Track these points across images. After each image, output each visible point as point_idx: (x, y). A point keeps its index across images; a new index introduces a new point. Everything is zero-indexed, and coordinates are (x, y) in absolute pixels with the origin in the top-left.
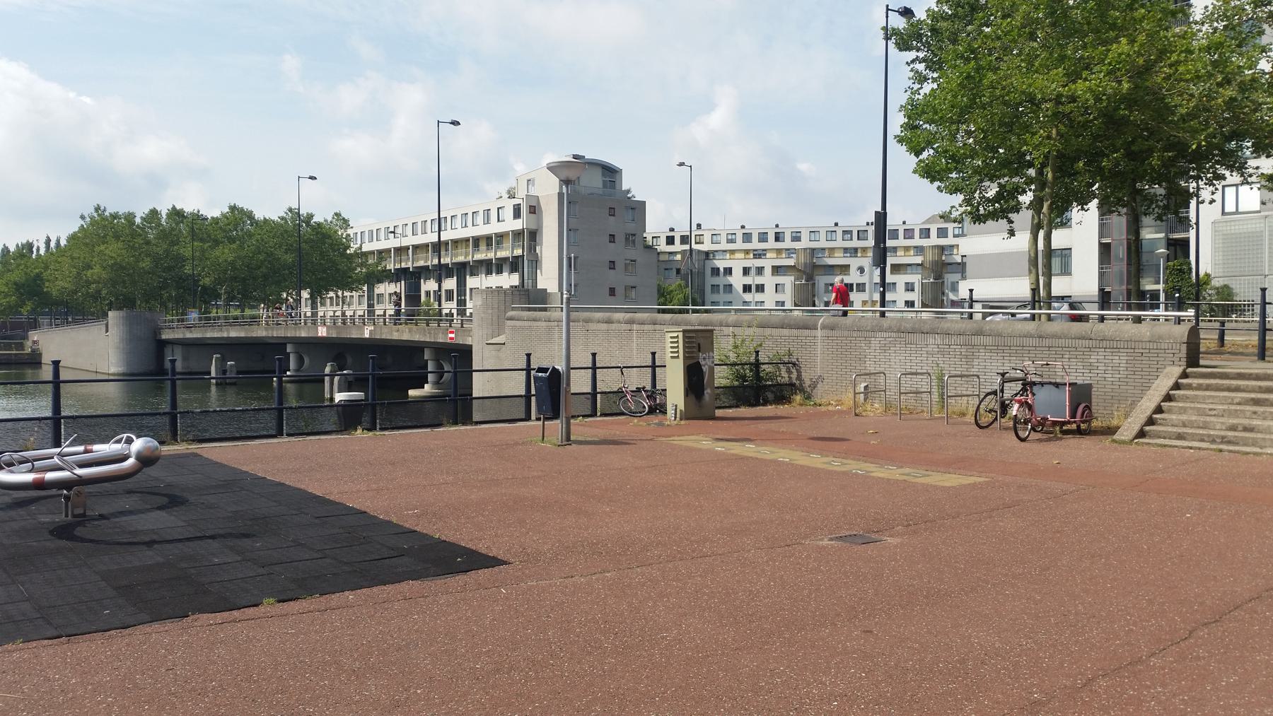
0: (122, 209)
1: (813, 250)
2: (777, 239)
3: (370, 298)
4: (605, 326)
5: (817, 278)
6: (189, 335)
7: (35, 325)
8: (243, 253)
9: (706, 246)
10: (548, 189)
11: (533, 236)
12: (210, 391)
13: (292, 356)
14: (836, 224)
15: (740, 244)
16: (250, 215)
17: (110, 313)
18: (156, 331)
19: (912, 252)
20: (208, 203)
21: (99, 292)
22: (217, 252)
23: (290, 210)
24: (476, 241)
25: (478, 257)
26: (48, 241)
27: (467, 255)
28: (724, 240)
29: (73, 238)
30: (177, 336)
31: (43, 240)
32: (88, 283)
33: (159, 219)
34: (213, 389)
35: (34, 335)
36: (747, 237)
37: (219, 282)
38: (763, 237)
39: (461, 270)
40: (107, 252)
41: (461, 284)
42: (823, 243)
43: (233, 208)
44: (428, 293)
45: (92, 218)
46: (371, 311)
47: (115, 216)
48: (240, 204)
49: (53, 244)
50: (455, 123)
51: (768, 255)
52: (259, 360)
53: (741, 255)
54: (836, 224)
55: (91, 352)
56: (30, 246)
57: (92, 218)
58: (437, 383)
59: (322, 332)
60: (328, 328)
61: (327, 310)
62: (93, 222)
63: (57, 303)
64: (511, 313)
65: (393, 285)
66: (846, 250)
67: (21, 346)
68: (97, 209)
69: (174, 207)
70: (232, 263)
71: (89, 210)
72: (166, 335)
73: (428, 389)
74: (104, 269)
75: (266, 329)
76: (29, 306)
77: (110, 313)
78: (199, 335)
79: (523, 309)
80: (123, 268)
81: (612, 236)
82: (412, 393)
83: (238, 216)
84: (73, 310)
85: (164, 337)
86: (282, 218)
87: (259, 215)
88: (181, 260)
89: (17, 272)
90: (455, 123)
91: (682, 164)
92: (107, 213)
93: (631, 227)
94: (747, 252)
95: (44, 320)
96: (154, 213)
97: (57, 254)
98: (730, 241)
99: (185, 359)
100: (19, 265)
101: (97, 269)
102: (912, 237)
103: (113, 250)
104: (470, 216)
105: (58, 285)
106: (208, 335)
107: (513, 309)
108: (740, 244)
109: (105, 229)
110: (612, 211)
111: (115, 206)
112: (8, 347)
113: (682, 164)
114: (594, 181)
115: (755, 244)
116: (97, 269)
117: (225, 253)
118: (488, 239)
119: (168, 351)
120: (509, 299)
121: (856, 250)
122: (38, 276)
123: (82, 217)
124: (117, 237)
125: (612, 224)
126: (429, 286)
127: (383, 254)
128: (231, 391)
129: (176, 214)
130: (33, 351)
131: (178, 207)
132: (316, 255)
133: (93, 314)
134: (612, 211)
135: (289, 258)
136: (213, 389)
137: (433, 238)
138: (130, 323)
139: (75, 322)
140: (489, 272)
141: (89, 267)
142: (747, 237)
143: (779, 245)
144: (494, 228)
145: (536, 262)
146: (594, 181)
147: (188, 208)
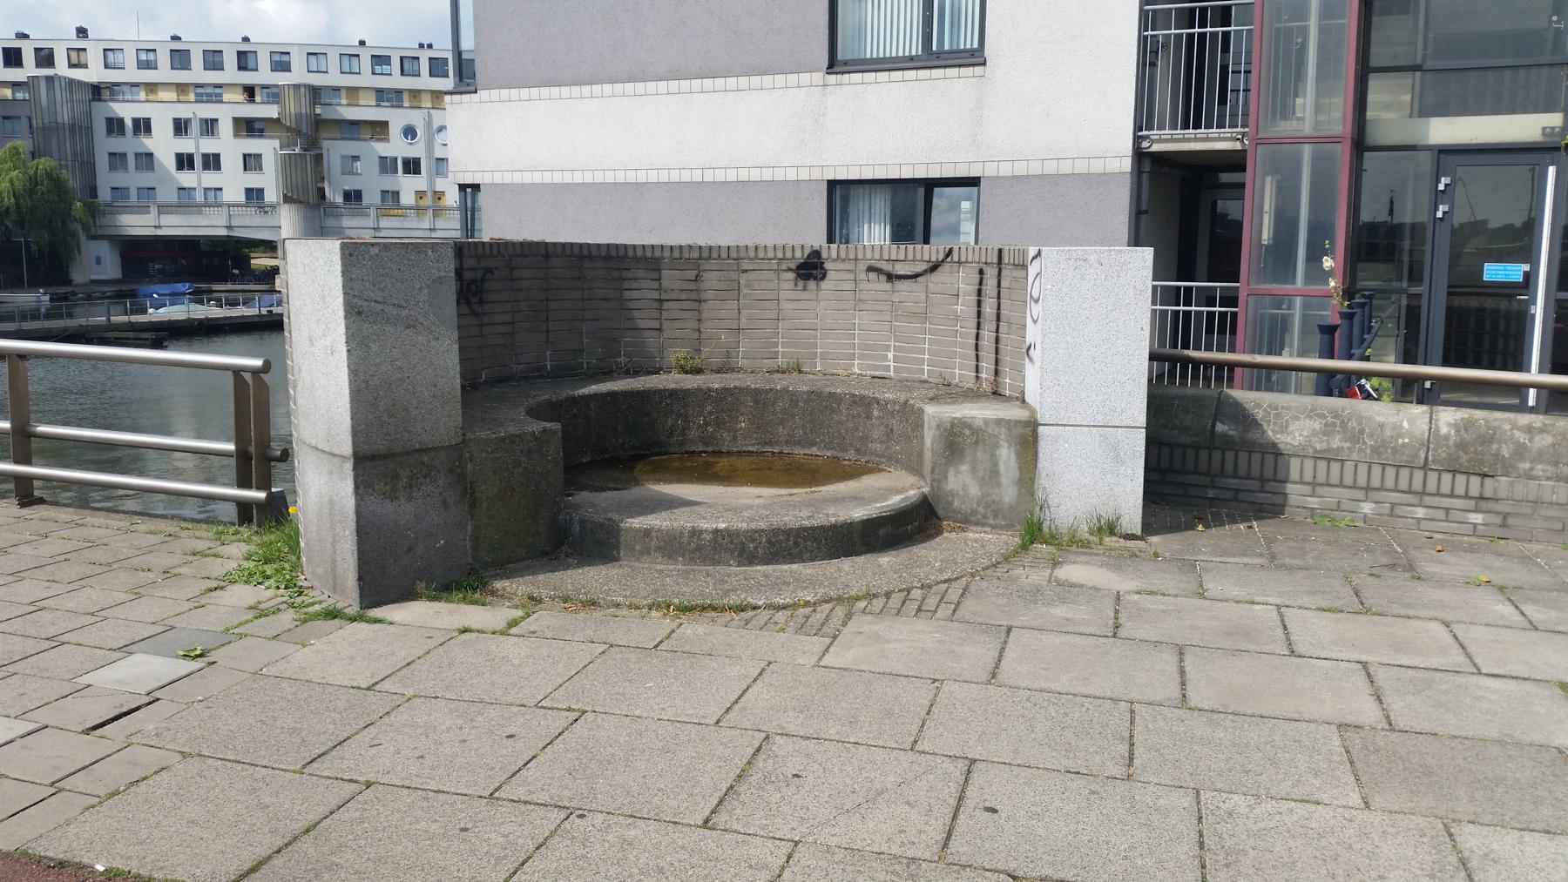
9: (94, 73)
42: (333, 78)
53: (172, 96)
54: (362, 43)
94: (182, 88)
108: (164, 73)
142: (180, 59)
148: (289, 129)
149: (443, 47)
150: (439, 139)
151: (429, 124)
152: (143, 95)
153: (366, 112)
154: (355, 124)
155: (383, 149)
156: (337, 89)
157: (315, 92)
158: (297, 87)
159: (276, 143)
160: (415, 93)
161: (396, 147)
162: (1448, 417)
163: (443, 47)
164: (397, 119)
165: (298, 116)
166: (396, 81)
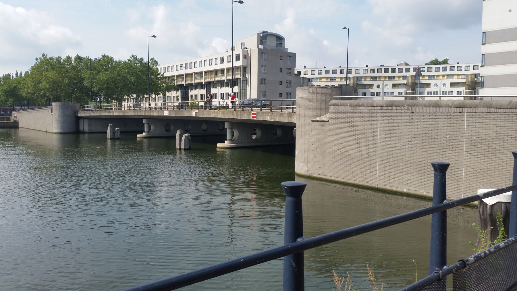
0: (55, 56)
1: (357, 77)
2: (385, 72)
3: (164, 98)
4: (432, 109)
5: (359, 90)
6: (92, 114)
7: (13, 110)
8: (112, 76)
9: (309, 76)
10: (253, 45)
11: (245, 69)
12: (105, 144)
13: (145, 125)
14: (367, 66)
15: (324, 75)
16: (111, 60)
17: (53, 104)
18: (76, 112)
19: (401, 79)
20: (94, 53)
21: (45, 94)
22: (100, 75)
23: (133, 56)
24: (216, 71)
25: (218, 79)
26: (17, 73)
27: (192, 80)
28: (317, 73)
29: (33, 69)
30: (86, 115)
31: (15, 73)
32: (40, 90)
33: (71, 61)
34: (109, 141)
35: (15, 114)
36: (327, 72)
37: (100, 90)
38: (334, 72)
39: (208, 85)
40: (49, 75)
41: (208, 91)
42: (361, 75)
43: (104, 56)
44: (192, 96)
45: (41, 59)
46: (164, 104)
47: (51, 59)
48: (107, 54)
49: (19, 75)
50: (154, 36)
51: (337, 80)
52: (129, 127)
53: (325, 80)
54: (367, 66)
55: (43, 123)
56: (9, 75)
57: (41, 59)
58: (232, 140)
59: (166, 113)
60: (170, 111)
61: (144, 104)
62: (42, 62)
63: (24, 99)
64: (333, 102)
65: (175, 92)
66: (372, 78)
67: (9, 119)
68: (43, 55)
69: (78, 55)
70: (107, 81)
71: (40, 56)
72: (80, 114)
73: (227, 144)
74: (48, 83)
75: (134, 112)
76: (11, 101)
77: (53, 104)
78: (98, 114)
79: (338, 99)
80: (57, 83)
81: (281, 69)
82: (219, 145)
83: (107, 60)
84: (31, 103)
85: (79, 115)
86: (129, 60)
87: (116, 59)
88: (82, 79)
89: (5, 86)
90: (154, 36)
91: (345, 28)
92: (48, 58)
93: (289, 65)
94: (327, 78)
95: (17, 107)
96: (69, 58)
97: (20, 79)
98: (319, 74)
99: (89, 126)
100: (6, 83)
101: (44, 83)
102: (402, 72)
103: (52, 74)
104: (193, 63)
105: (23, 93)
106: (103, 114)
107: (334, 99)
108: (324, 75)
109: (47, 65)
110: (281, 58)
111: (52, 54)
112: (3, 119)
113: (345, 28)
114: (272, 43)
115: (331, 75)
116: (44, 83)
117: (103, 76)
118: (201, 73)
119: (81, 122)
120: (329, 92)
121: (376, 77)
122: (15, 87)
123: (37, 59)
124: (53, 69)
125: (281, 64)
126: (192, 92)
127: (171, 78)
128: (117, 142)
129: (79, 59)
130: (15, 121)
131: (80, 55)
132: (142, 78)
133: (39, 105)
134: (281, 58)
135: (133, 79)
136: (109, 141)
137: (230, 65)
138: (63, 108)
139: (35, 108)
140: (222, 86)
141: (40, 82)
142: (327, 72)
143: (327, 76)
144: (220, 66)
145: (246, 81)
146: (272, 43)
147: (84, 56)
148: (467, 85)
149: (344, 67)
150: (385, 88)
151: (383, 84)
152: (318, 80)
153: (368, 82)
154: (365, 85)
155: (372, 91)
156: (362, 77)
157: (476, 75)
158: (354, 77)
159: (464, 88)
160: (380, 77)
161: (375, 90)
162: (5, 130)
163: (344, 67)
164: (375, 83)
165: (354, 84)
166: (376, 74)
